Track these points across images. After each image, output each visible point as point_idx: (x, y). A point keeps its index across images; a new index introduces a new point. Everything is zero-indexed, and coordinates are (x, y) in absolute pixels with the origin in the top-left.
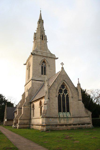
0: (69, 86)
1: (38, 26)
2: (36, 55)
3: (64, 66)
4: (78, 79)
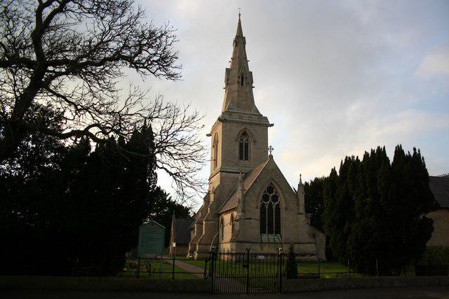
0: (281, 189)
1: (235, 52)
2: (229, 121)
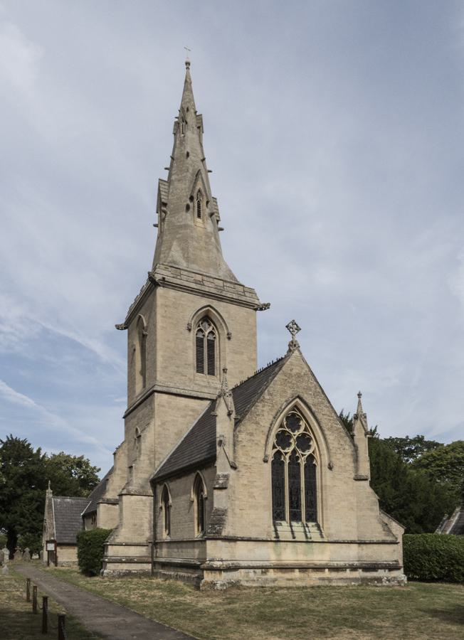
3: (299, 338)
4: (359, 395)
